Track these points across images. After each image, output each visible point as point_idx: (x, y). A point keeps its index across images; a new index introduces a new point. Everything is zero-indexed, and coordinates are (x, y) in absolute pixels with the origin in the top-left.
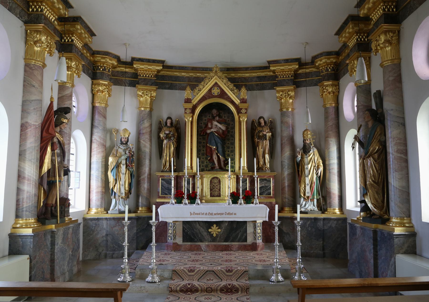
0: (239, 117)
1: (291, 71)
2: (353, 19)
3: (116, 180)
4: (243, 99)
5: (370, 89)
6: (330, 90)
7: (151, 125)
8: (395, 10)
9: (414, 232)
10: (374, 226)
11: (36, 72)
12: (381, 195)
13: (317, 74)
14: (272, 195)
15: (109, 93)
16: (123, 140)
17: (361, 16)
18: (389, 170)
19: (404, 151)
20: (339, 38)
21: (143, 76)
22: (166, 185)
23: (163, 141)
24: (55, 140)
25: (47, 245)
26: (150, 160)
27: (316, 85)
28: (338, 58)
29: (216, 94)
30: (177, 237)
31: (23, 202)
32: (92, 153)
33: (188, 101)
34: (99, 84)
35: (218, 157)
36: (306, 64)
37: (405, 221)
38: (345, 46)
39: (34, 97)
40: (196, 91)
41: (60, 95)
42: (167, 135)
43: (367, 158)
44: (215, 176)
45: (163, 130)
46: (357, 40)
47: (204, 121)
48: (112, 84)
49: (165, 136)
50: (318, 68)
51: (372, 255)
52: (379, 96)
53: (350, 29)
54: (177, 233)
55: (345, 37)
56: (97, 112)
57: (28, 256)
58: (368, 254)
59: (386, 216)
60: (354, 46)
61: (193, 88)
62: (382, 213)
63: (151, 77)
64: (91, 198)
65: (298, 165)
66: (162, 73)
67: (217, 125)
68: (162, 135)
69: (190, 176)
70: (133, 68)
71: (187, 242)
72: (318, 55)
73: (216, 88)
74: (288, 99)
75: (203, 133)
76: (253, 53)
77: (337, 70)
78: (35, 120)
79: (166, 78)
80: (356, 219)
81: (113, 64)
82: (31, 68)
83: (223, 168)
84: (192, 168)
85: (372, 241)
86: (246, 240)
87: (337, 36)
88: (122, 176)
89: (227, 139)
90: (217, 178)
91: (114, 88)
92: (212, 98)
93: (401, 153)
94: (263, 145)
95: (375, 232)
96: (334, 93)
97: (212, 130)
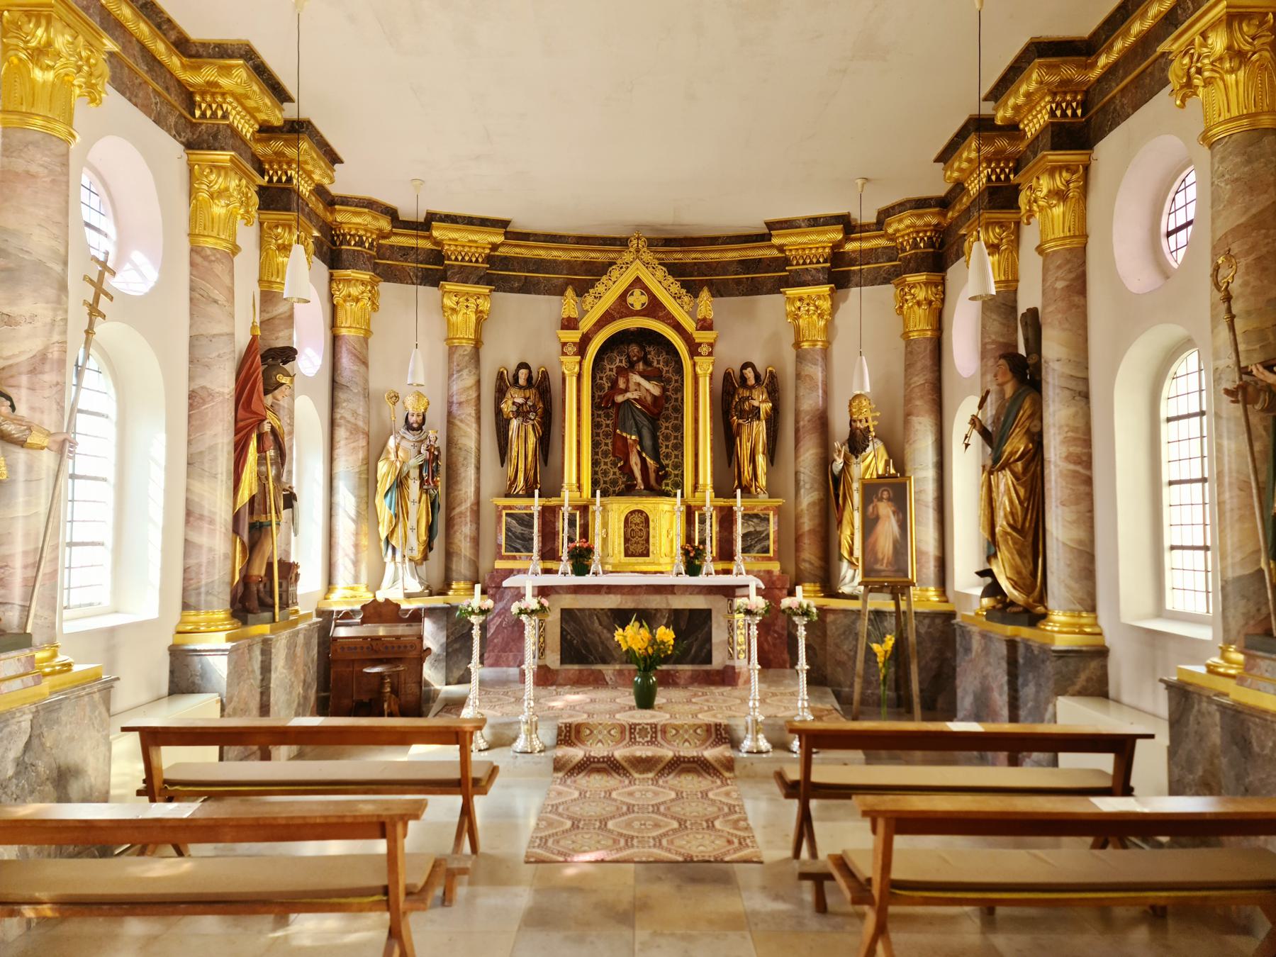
0: (694, 365)
1: (824, 248)
2: (979, 126)
3: (396, 516)
4: (704, 320)
5: (1015, 301)
6: (921, 294)
7: (478, 382)
8: (1079, 112)
9: (1104, 646)
10: (1010, 630)
11: (219, 268)
12: (1030, 558)
13: (890, 254)
14: (771, 554)
15: (373, 303)
16: (412, 419)
17: (999, 123)
18: (1047, 501)
19: (1084, 458)
20: (945, 170)
21: (456, 259)
22: (518, 529)
23: (508, 421)
24: (267, 428)
25: (253, 671)
26: (478, 469)
27: (886, 281)
28: (945, 216)
29: (638, 307)
30: (547, 652)
31: (198, 573)
32: (337, 452)
33: (569, 324)
34: (348, 281)
35: (643, 461)
36: (864, 228)
37: (1083, 621)
38: (959, 188)
39: (217, 329)
40: (589, 299)
41: (267, 316)
42: (519, 406)
43: (999, 470)
44: (640, 507)
45: (508, 395)
46: (989, 177)
47: (608, 373)
48: (378, 279)
49: (515, 408)
50: (892, 238)
51: (1005, 698)
52: (1033, 321)
53: (970, 151)
54: (548, 641)
55: (960, 170)
56: (344, 349)
57: (215, 697)
58: (996, 695)
59: (1040, 609)
60: (980, 194)
61: (582, 290)
62: (1031, 600)
63: (477, 261)
64: (334, 560)
65: (837, 480)
66: (502, 251)
67: (639, 384)
68: (507, 407)
69: (576, 507)
70: (429, 237)
71: (572, 662)
72: (893, 207)
73: (637, 292)
74: (815, 317)
75: (607, 403)
76: (730, 204)
77: (942, 245)
78: (223, 381)
79: (518, 263)
80: (972, 614)
81: (380, 230)
82: (206, 258)
83: (654, 490)
84: (579, 488)
85: (1004, 665)
86: (708, 659)
87: (941, 165)
88: (413, 509)
89: (662, 415)
90: (641, 512)
91: (388, 290)
92: (627, 316)
93: (1075, 463)
94: (750, 434)
95: (1012, 644)
96: (930, 303)
97: (629, 395)
